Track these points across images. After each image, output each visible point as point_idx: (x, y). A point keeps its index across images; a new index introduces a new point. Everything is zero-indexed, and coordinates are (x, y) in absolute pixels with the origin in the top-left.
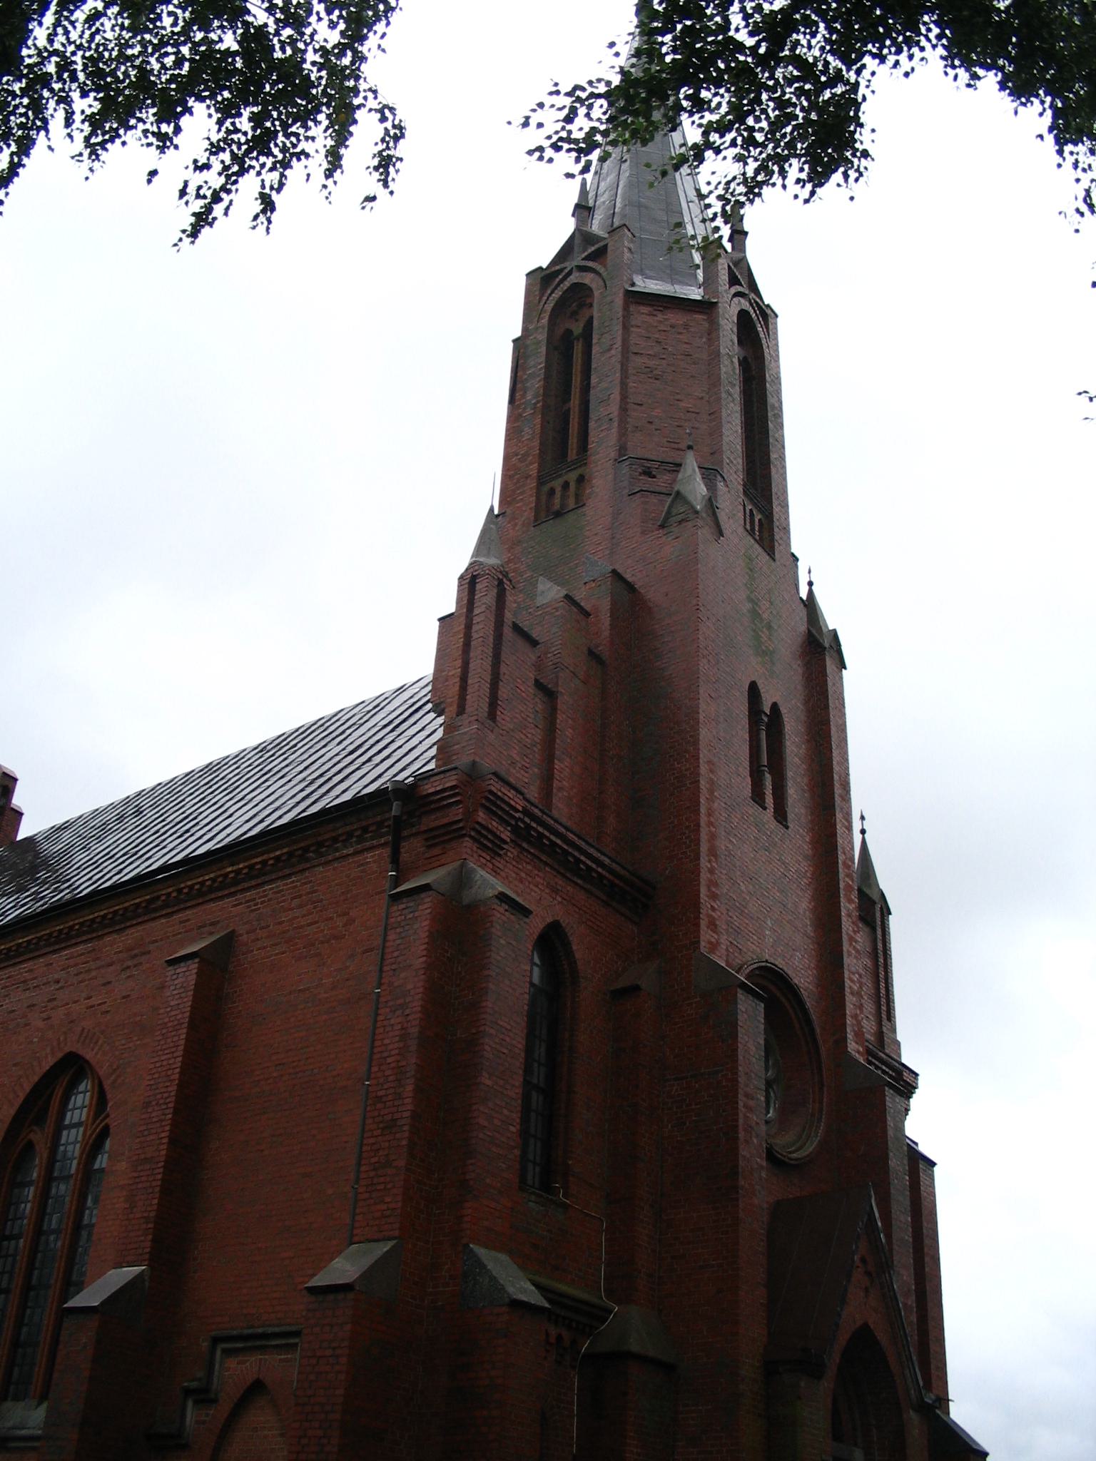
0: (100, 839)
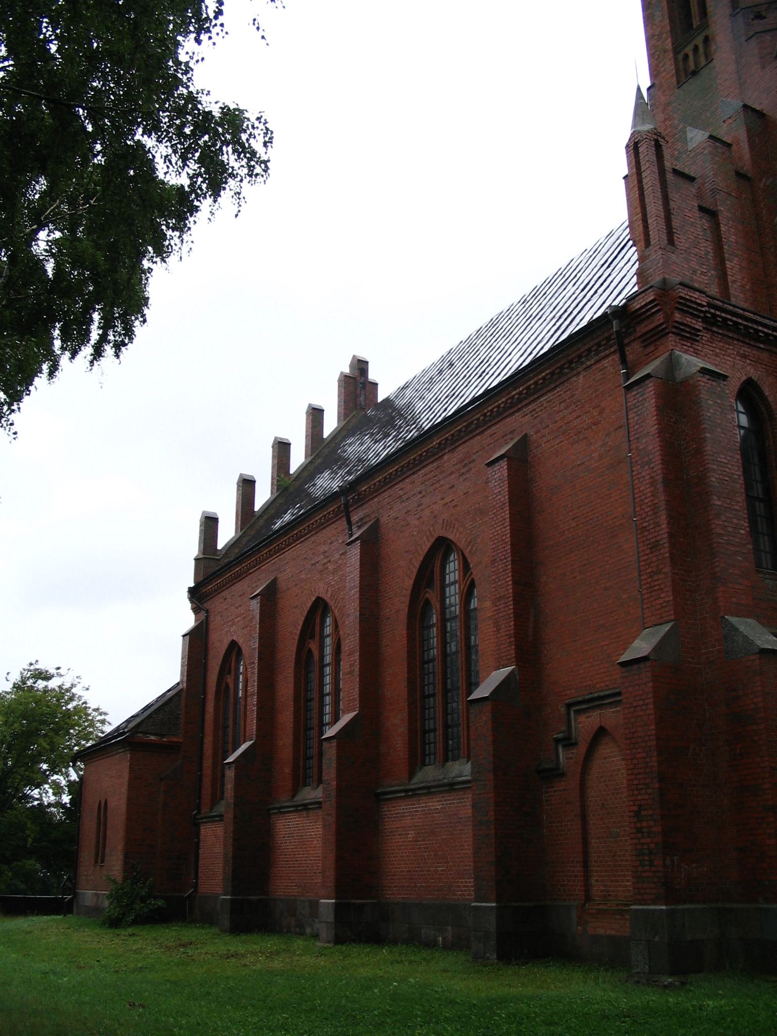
0: (429, 390)
